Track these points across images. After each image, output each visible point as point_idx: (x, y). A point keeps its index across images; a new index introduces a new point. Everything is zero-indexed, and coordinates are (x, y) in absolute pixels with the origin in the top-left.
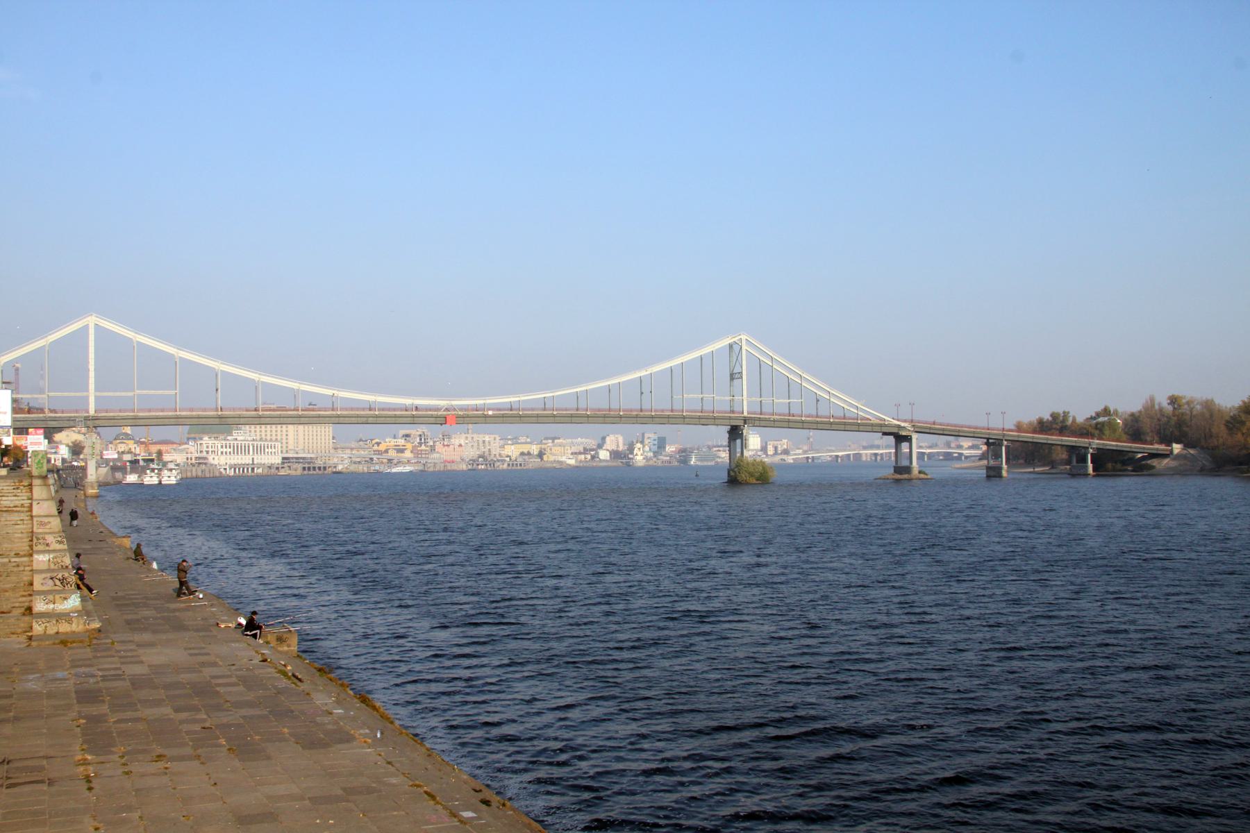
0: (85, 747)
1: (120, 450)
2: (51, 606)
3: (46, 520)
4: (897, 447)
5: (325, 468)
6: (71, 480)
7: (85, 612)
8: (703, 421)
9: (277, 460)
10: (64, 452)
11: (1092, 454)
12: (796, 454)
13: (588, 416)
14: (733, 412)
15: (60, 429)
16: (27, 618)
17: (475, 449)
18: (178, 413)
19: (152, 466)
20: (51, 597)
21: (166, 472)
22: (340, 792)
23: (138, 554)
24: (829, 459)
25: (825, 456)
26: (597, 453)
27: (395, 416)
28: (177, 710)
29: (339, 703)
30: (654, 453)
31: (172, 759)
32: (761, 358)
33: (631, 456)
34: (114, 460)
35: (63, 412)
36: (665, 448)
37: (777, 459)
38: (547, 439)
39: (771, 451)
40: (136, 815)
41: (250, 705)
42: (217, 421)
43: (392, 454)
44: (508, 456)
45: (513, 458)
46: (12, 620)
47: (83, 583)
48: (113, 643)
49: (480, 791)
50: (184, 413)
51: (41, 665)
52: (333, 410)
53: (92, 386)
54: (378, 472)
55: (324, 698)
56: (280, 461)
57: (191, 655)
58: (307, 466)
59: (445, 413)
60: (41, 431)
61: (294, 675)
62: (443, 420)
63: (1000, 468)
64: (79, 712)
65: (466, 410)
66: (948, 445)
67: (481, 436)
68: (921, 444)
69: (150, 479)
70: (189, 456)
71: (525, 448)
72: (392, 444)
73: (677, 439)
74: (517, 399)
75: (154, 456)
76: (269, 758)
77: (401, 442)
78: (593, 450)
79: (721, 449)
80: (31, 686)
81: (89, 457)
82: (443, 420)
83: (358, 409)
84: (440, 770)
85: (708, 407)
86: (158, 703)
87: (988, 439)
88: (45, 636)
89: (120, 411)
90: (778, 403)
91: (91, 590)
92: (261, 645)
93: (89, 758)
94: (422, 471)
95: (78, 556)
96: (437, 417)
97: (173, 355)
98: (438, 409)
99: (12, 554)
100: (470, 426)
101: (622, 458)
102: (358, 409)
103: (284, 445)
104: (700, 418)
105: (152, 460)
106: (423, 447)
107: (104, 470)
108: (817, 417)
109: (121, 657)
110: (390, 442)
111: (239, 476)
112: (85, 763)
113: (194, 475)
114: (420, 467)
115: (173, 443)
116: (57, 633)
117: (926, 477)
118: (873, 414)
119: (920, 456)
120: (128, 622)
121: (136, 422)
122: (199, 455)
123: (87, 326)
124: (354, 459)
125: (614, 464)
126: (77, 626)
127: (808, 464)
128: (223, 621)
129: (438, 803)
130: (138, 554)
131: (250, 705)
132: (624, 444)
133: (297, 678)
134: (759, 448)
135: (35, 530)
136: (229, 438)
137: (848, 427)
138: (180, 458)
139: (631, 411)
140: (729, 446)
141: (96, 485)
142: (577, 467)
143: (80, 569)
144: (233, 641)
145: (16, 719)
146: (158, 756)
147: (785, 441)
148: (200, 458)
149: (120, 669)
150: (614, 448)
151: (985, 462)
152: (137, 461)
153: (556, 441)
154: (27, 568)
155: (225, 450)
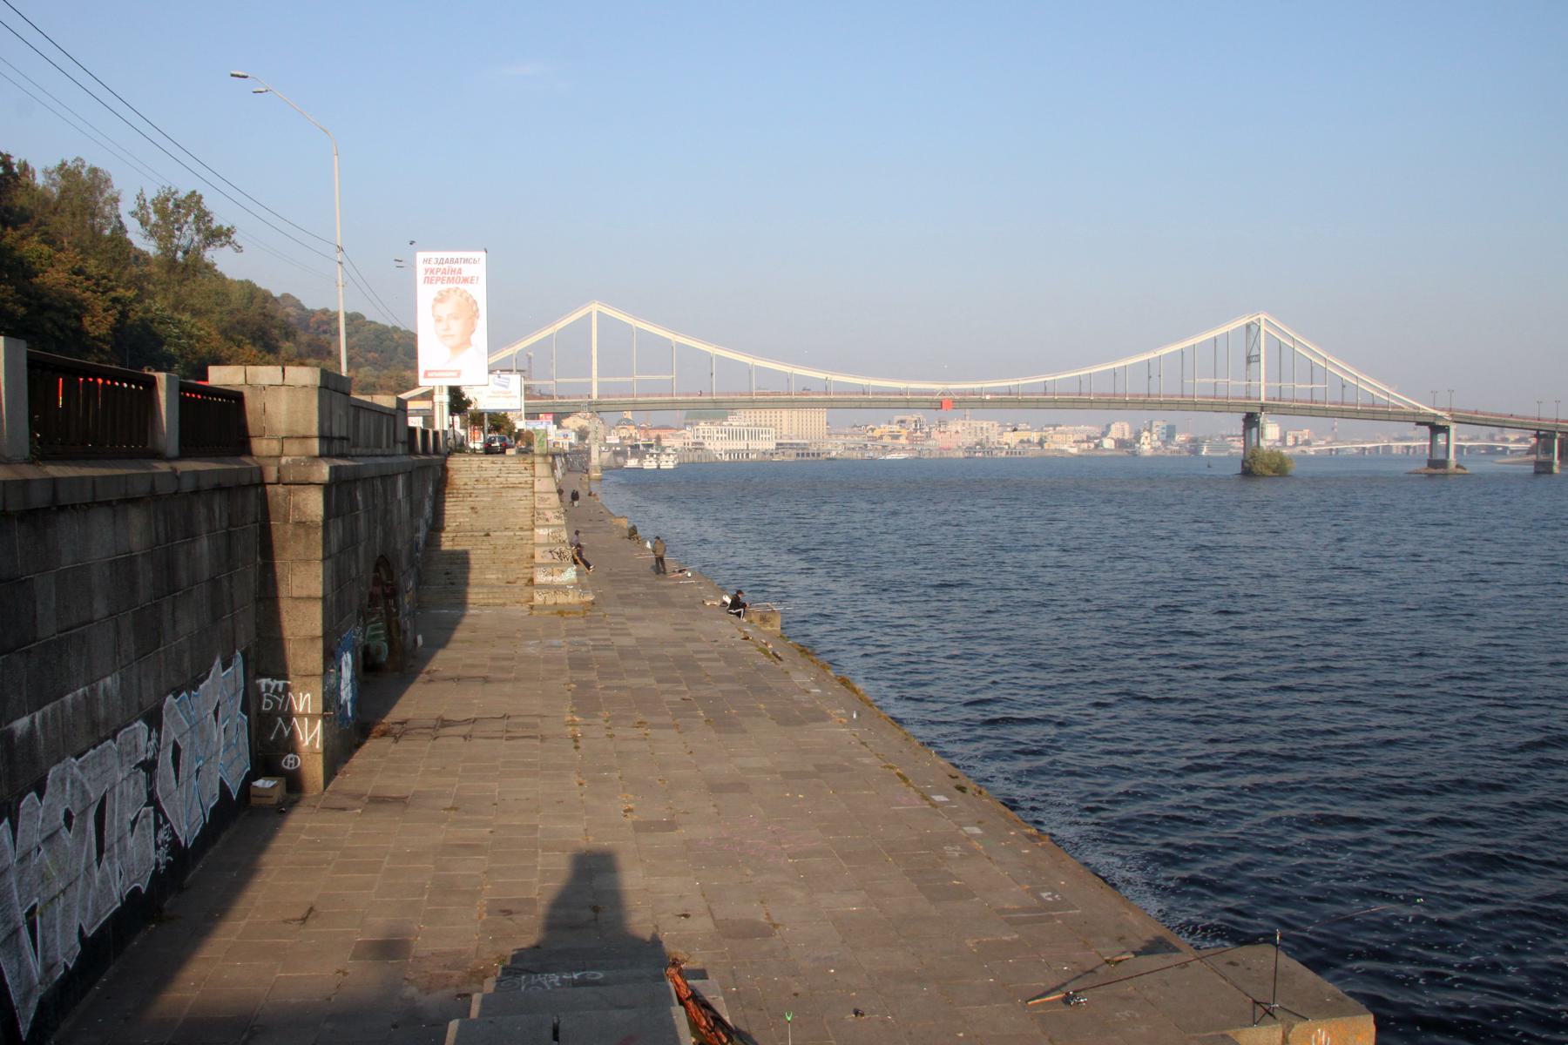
0: (574, 709)
1: (622, 435)
2: (550, 578)
3: (546, 496)
4: (1433, 439)
5: (819, 454)
6: (577, 464)
7: (579, 585)
8: (1215, 408)
9: (771, 446)
10: (573, 439)
11: (1561, 441)
12: (1318, 446)
13: (1092, 402)
14: (1249, 398)
15: (567, 415)
16: (529, 589)
17: (972, 436)
18: (675, 398)
19: (651, 451)
20: (549, 569)
21: (664, 457)
22: (812, 769)
23: (633, 532)
24: (1355, 451)
25: (1351, 448)
26: (1101, 442)
27: (889, 401)
28: (659, 681)
29: (817, 683)
30: (1163, 442)
31: (653, 726)
32: (1282, 340)
33: (1137, 445)
34: (616, 445)
35: (569, 398)
36: (1174, 437)
37: (1298, 450)
38: (1047, 426)
39: (1290, 442)
40: (616, 775)
41: (730, 680)
42: (712, 406)
43: (887, 440)
44: (1006, 444)
45: (1012, 446)
46: (517, 590)
47: (579, 558)
48: (605, 616)
49: (957, 777)
50: (679, 398)
51: (541, 632)
52: (826, 394)
53: (595, 373)
54: (872, 459)
55: (802, 678)
56: (774, 447)
57: (676, 630)
58: (800, 452)
59: (940, 397)
60: (551, 416)
61: (774, 654)
62: (939, 405)
63: (1551, 464)
64: (571, 677)
65: (962, 394)
66: (1492, 438)
67: (979, 422)
68: (1461, 436)
69: (649, 464)
70: (686, 441)
71: (1024, 436)
72: (887, 430)
73: (1357, 440)
74: (1016, 383)
75: (653, 442)
76: (744, 731)
77: (896, 428)
78: (1097, 438)
79: (1236, 439)
80: (530, 650)
81: (592, 441)
82: (939, 405)
83: (851, 393)
84: (915, 754)
85: (1221, 392)
86: (643, 674)
87: (1538, 431)
88: (544, 607)
89: (621, 396)
90: (1299, 389)
91: (588, 566)
92: (744, 624)
93: (577, 719)
94: (916, 458)
95: (577, 533)
96: (932, 401)
97: (669, 340)
98: (933, 393)
99: (517, 527)
100: (968, 411)
101: (1126, 447)
102: (851, 393)
103: (779, 431)
104: (1212, 404)
105: (651, 446)
106: (919, 434)
107: (606, 455)
108: (1343, 404)
109: (611, 629)
110: (884, 428)
111: (734, 462)
112: (573, 724)
113: (691, 460)
114: (916, 455)
115: (671, 428)
116: (556, 604)
117: (1463, 471)
118: (1406, 402)
119: (1459, 449)
120: (620, 597)
121: (635, 407)
122: (696, 440)
123: (589, 315)
124: (848, 446)
125: (1119, 453)
126: (572, 598)
127: (1331, 457)
128: (709, 600)
129: (909, 785)
130: (633, 532)
131: (730, 680)
132: (1130, 433)
133: (777, 657)
134: (1277, 437)
135: (537, 506)
136: (725, 423)
137: (1377, 416)
138: (677, 443)
139: (1138, 396)
140: (1244, 435)
141: (599, 469)
142: (1080, 456)
143: (579, 545)
144: (717, 619)
145: (517, 679)
146: (640, 723)
147: (1306, 431)
148: (696, 443)
149: (609, 640)
150: (1120, 436)
151: (1533, 457)
152: (637, 446)
153: (1058, 428)
154: (530, 542)
155: (720, 435)
